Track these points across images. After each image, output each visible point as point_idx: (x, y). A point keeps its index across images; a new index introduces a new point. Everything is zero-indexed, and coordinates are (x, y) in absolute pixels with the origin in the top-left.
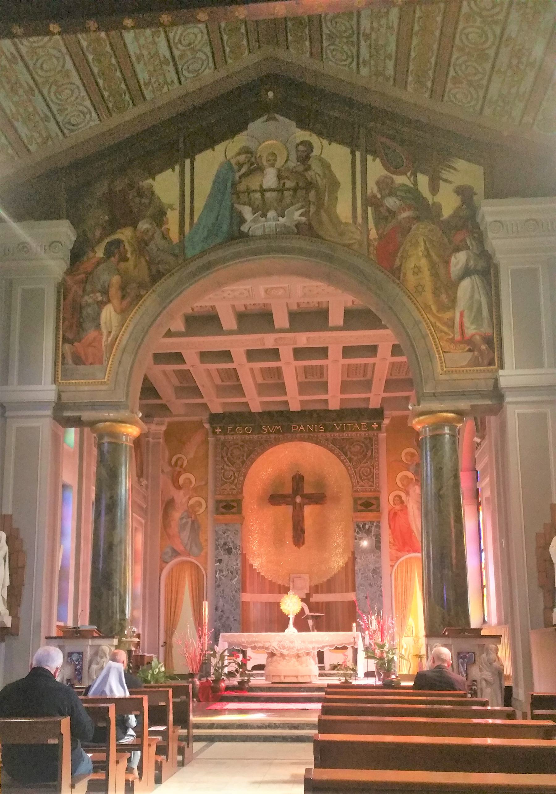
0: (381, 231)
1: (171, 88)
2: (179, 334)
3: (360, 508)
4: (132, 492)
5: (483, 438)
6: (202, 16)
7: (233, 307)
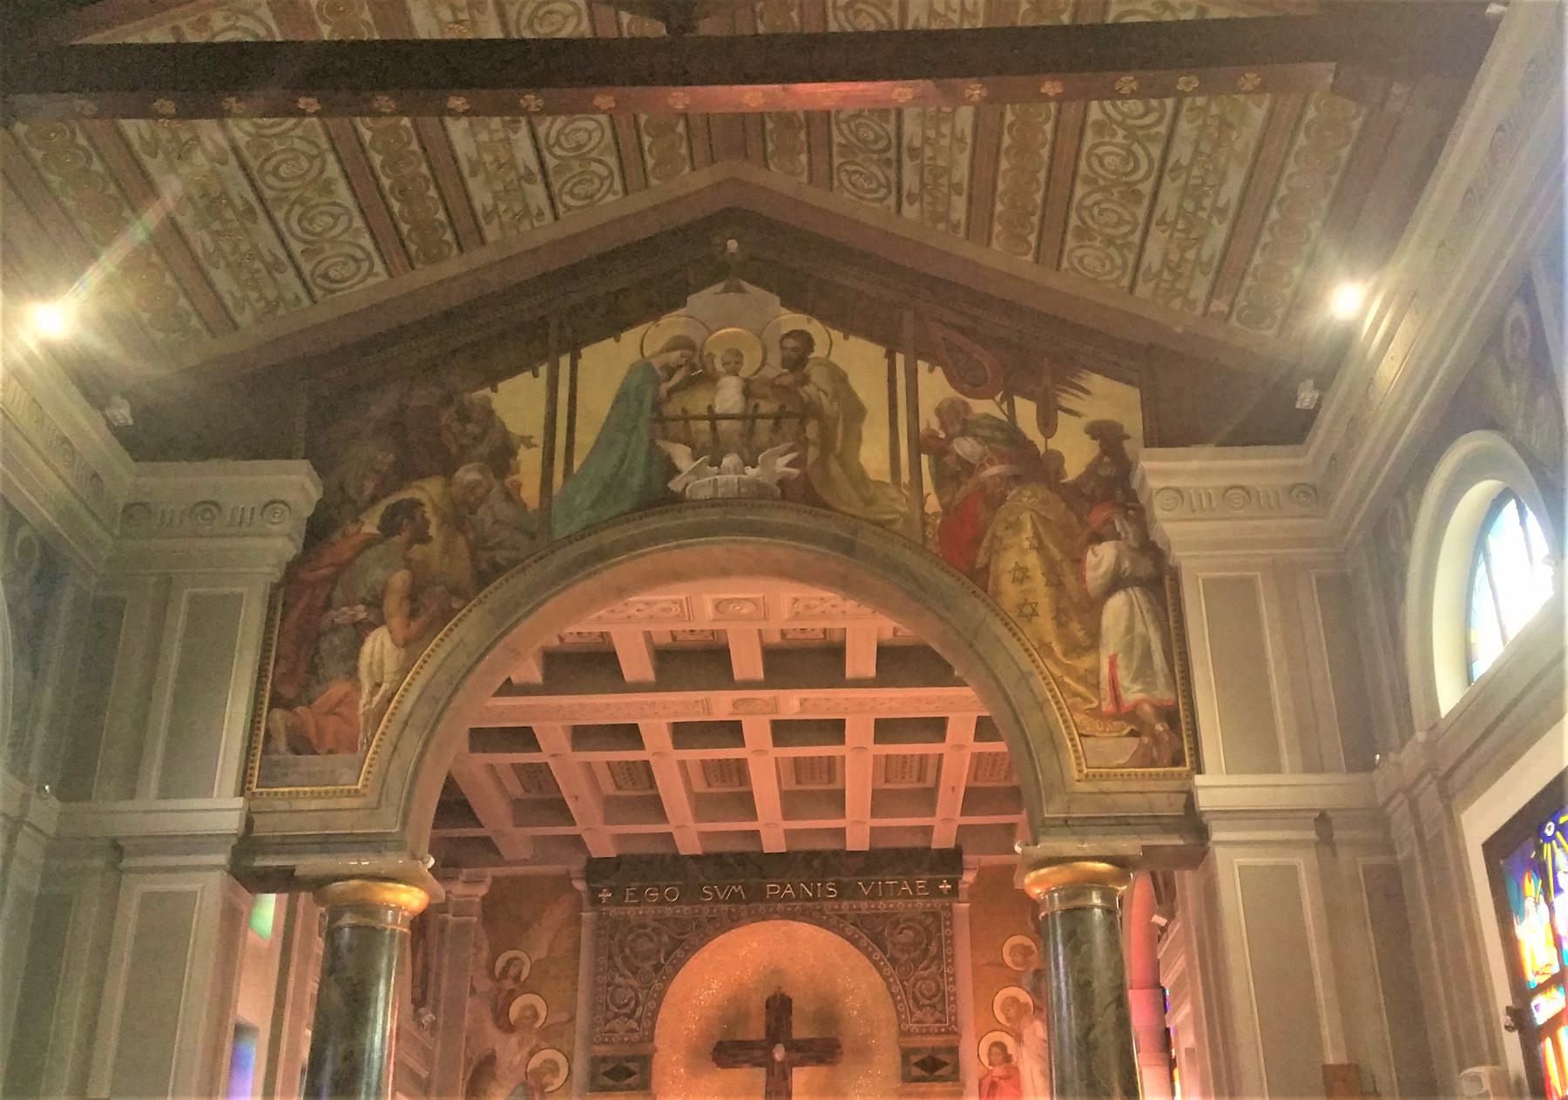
0: (947, 499)
1: (536, 224)
2: (526, 690)
3: (916, 1071)
4: (397, 1040)
5: (1171, 916)
6: (604, 100)
7: (648, 636)
